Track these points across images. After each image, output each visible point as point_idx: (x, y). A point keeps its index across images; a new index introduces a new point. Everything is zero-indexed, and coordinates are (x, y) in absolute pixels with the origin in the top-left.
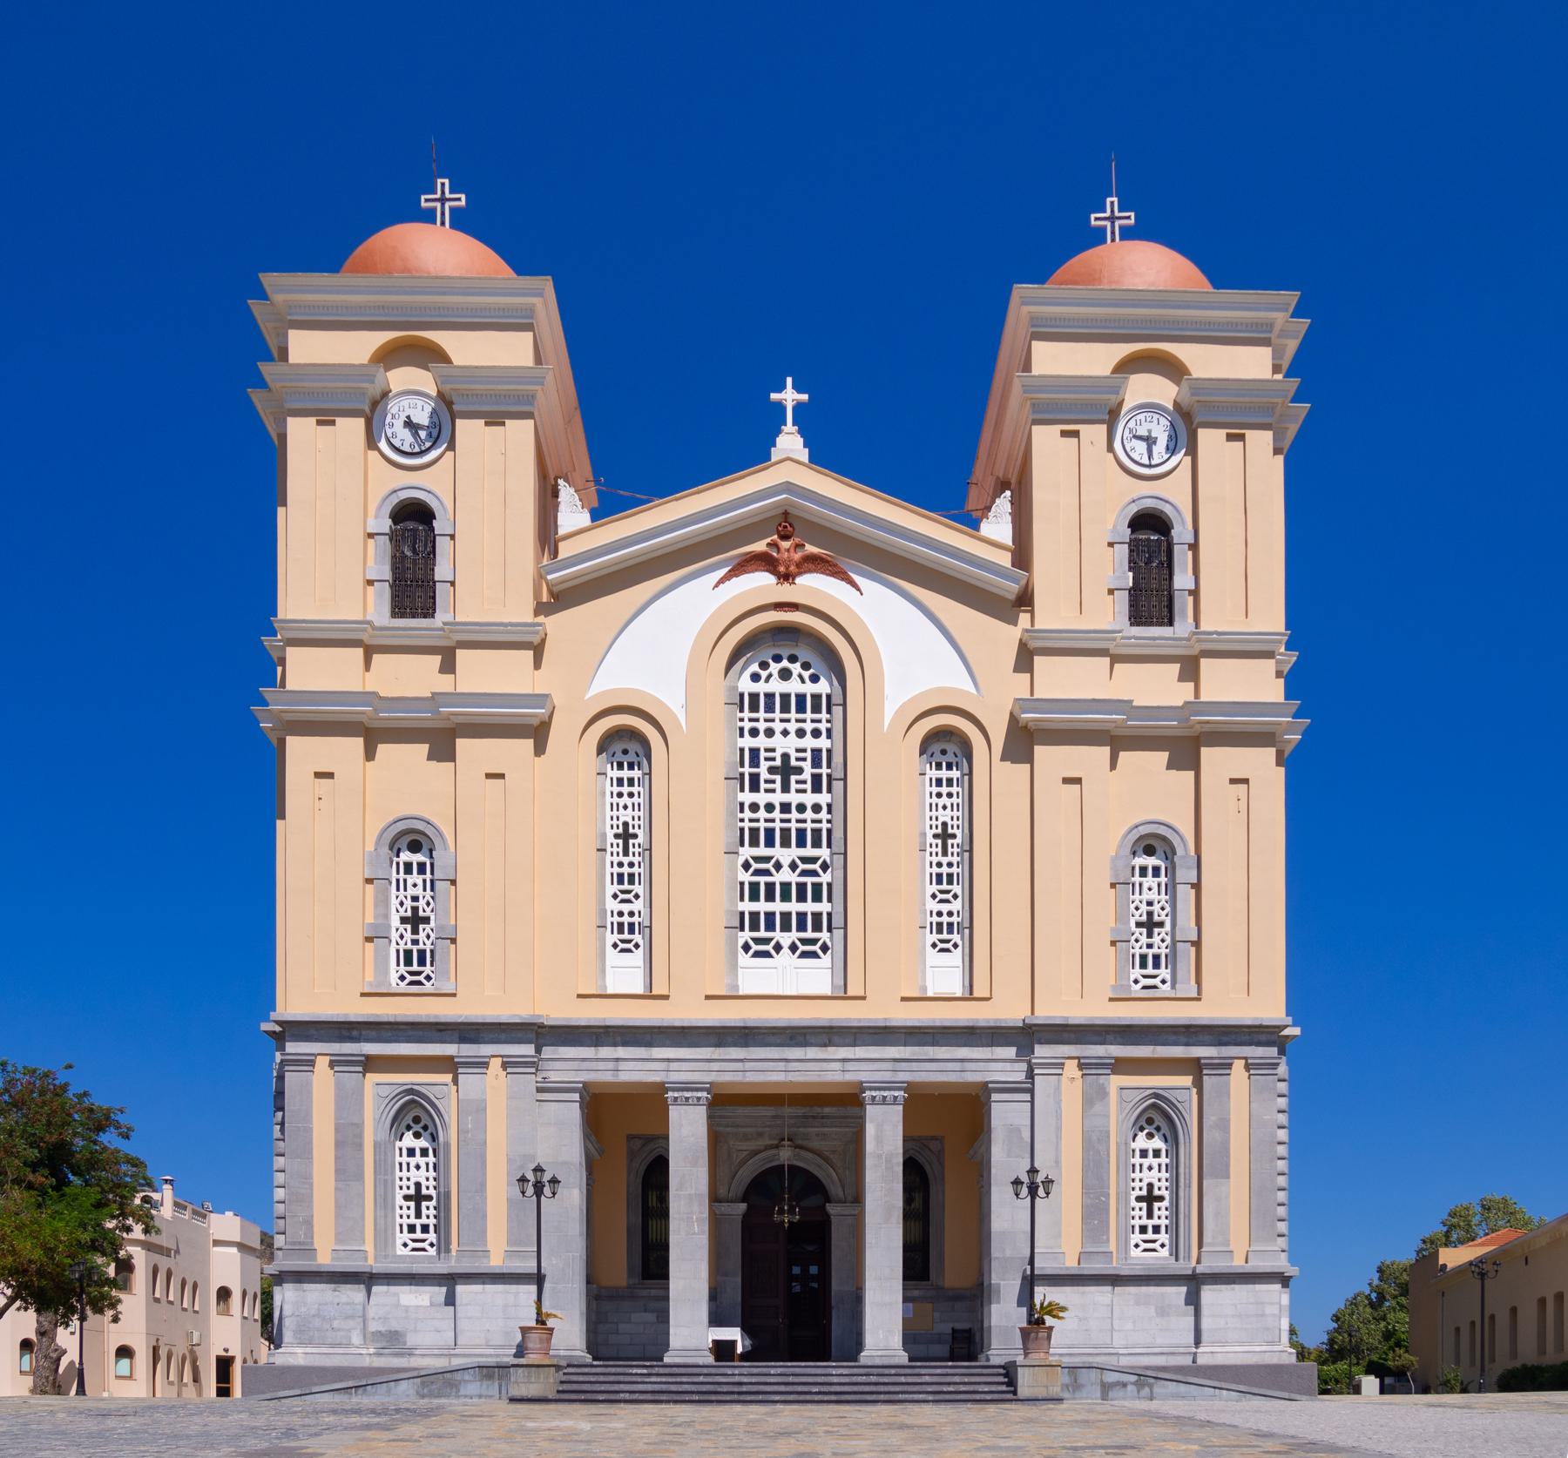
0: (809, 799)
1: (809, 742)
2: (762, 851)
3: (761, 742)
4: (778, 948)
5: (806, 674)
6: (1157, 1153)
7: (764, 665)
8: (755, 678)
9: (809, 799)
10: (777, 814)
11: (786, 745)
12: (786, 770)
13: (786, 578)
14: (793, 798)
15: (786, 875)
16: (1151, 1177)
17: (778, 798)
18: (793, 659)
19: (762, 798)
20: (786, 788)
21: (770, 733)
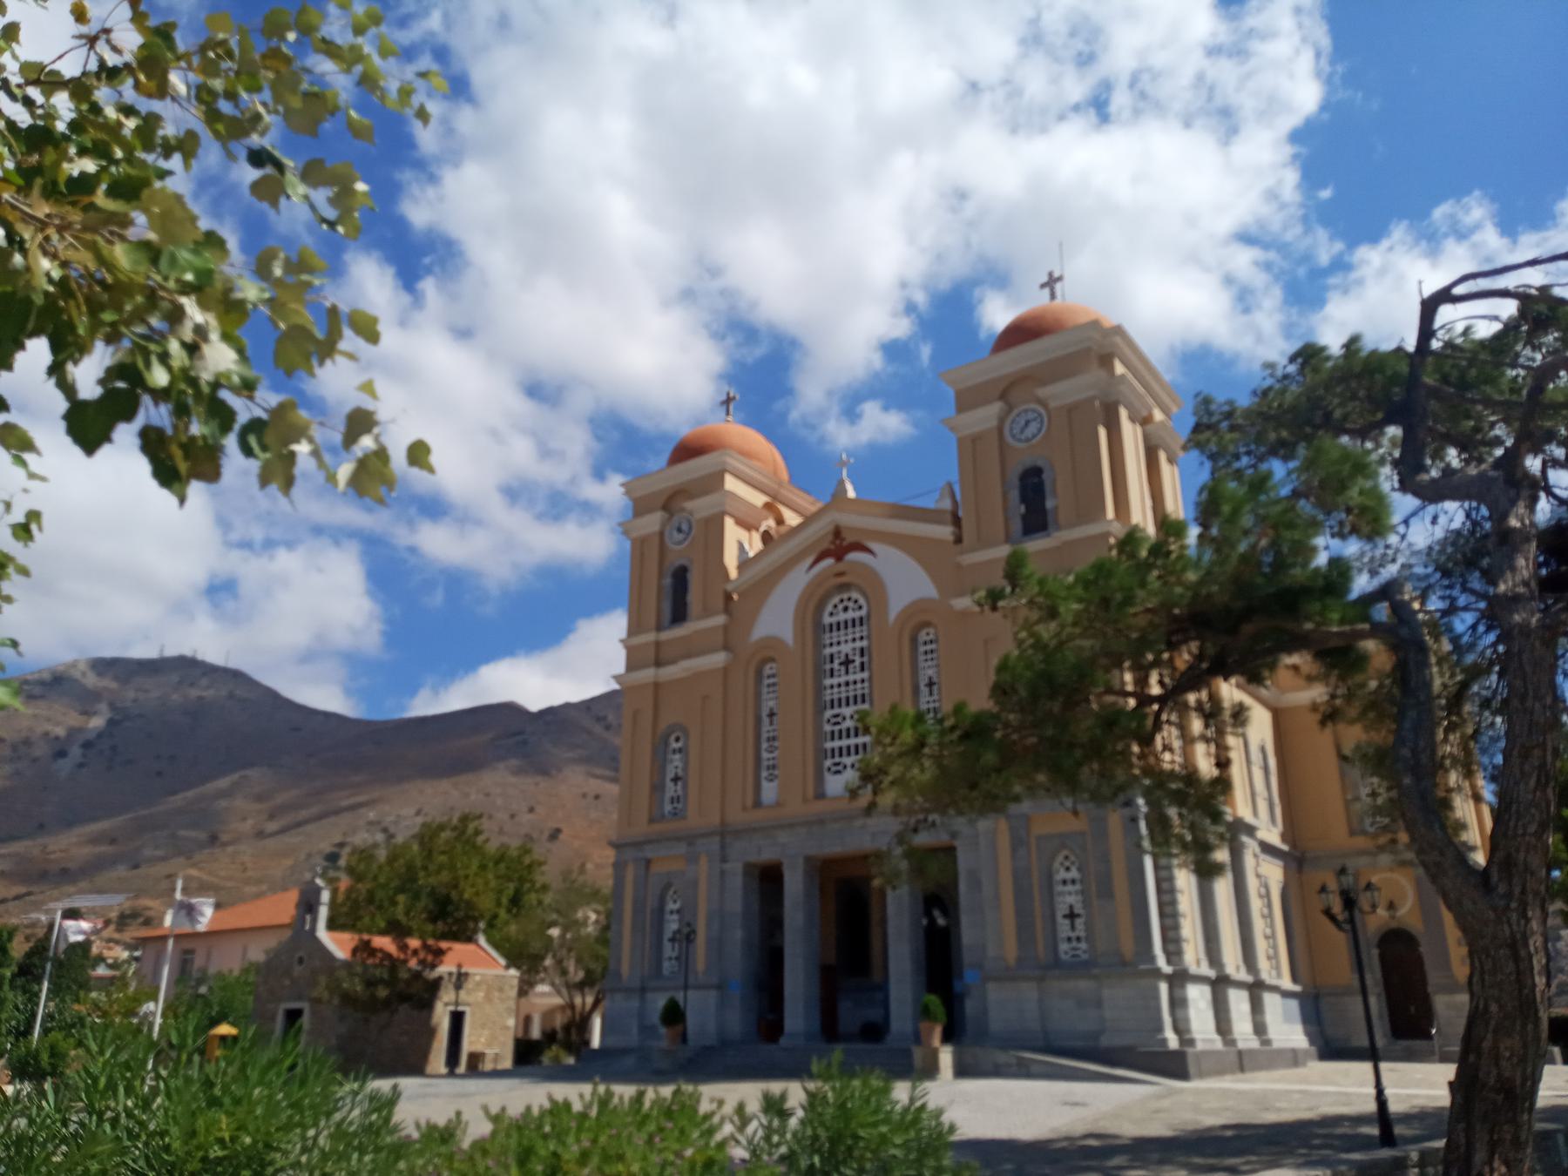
0: (859, 676)
1: (858, 644)
2: (836, 711)
3: (835, 649)
4: (845, 767)
5: (856, 606)
6: (1073, 882)
7: (835, 606)
8: (831, 614)
9: (859, 676)
10: (843, 689)
11: (846, 648)
12: (847, 662)
13: (839, 558)
14: (851, 678)
15: (849, 723)
16: (1071, 899)
17: (843, 679)
18: (849, 599)
19: (835, 681)
20: (847, 672)
21: (839, 643)
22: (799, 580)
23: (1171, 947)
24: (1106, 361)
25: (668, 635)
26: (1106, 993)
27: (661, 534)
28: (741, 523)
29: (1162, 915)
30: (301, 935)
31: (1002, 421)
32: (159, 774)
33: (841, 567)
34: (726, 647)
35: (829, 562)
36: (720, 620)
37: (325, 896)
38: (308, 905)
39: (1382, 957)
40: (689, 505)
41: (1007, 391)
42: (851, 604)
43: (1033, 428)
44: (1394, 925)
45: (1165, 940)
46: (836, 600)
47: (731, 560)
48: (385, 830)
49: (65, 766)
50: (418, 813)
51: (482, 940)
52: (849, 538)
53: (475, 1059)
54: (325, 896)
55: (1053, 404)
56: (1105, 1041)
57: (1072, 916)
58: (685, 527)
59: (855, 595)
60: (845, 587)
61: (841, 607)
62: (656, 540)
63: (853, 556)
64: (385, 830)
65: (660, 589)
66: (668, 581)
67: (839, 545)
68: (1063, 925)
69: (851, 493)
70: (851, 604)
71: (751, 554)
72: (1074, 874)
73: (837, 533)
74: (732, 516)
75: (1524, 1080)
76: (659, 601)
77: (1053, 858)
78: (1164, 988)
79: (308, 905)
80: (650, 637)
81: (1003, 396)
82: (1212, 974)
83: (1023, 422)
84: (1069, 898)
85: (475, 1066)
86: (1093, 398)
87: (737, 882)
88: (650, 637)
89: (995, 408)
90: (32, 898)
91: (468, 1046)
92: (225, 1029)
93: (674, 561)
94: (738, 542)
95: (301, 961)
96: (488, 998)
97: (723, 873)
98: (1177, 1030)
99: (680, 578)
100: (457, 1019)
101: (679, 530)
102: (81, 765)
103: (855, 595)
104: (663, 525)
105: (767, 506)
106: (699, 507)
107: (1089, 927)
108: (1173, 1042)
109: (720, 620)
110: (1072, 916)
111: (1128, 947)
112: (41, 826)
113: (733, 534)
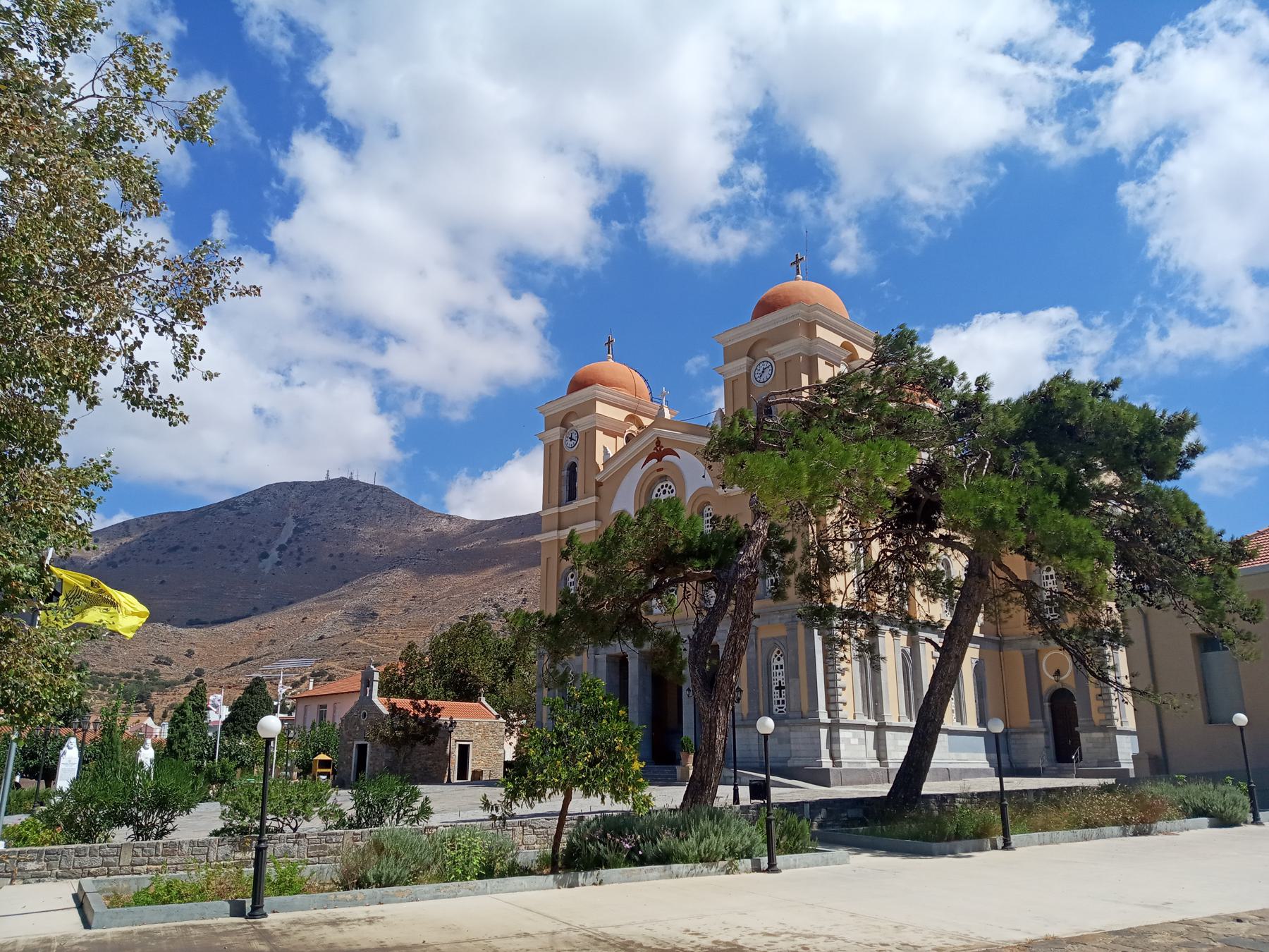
7: (659, 490)
13: (659, 460)
22: (638, 472)
23: (832, 707)
24: (810, 329)
25: (564, 509)
26: (792, 735)
27: (561, 441)
28: (606, 433)
29: (827, 687)
30: (366, 700)
31: (749, 368)
32: (334, 568)
33: (660, 465)
34: (597, 519)
35: (654, 461)
36: (593, 499)
37: (376, 676)
38: (367, 682)
39: (1052, 707)
40: (771, 351)
41: (752, 350)
42: (667, 489)
43: (767, 372)
44: (1059, 686)
45: (828, 703)
46: (659, 486)
47: (599, 460)
48: (496, 606)
49: (267, 565)
50: (519, 592)
51: (483, 700)
52: (665, 446)
53: (477, 775)
54: (376, 676)
55: (777, 359)
56: (790, 764)
57: (780, 688)
58: (574, 437)
59: (670, 484)
60: (664, 478)
61: (662, 490)
62: (557, 446)
63: (667, 458)
64: (496, 606)
65: (561, 477)
66: (565, 473)
67: (660, 451)
68: (775, 693)
69: (667, 415)
70: (667, 489)
71: (611, 455)
72: (782, 662)
73: (658, 442)
74: (600, 429)
75: (708, 776)
76: (560, 486)
77: (771, 651)
78: (824, 733)
79: (367, 682)
80: (555, 510)
81: (563, 425)
82: (873, 722)
83: (762, 370)
84: (778, 677)
85: (477, 777)
86: (799, 354)
87: (603, 667)
88: (555, 510)
89: (744, 361)
90: (252, 662)
91: (471, 768)
92: (322, 757)
93: (569, 459)
94: (606, 445)
95: (365, 714)
96: (484, 737)
97: (596, 660)
98: (832, 757)
99: (572, 468)
100: (464, 750)
101: (571, 439)
102: (279, 563)
103: (670, 484)
104: (562, 436)
105: (629, 418)
106: (580, 424)
107: (788, 695)
108: (826, 763)
109: (593, 499)
110: (780, 688)
111: (805, 707)
112: (255, 609)
113: (602, 440)
